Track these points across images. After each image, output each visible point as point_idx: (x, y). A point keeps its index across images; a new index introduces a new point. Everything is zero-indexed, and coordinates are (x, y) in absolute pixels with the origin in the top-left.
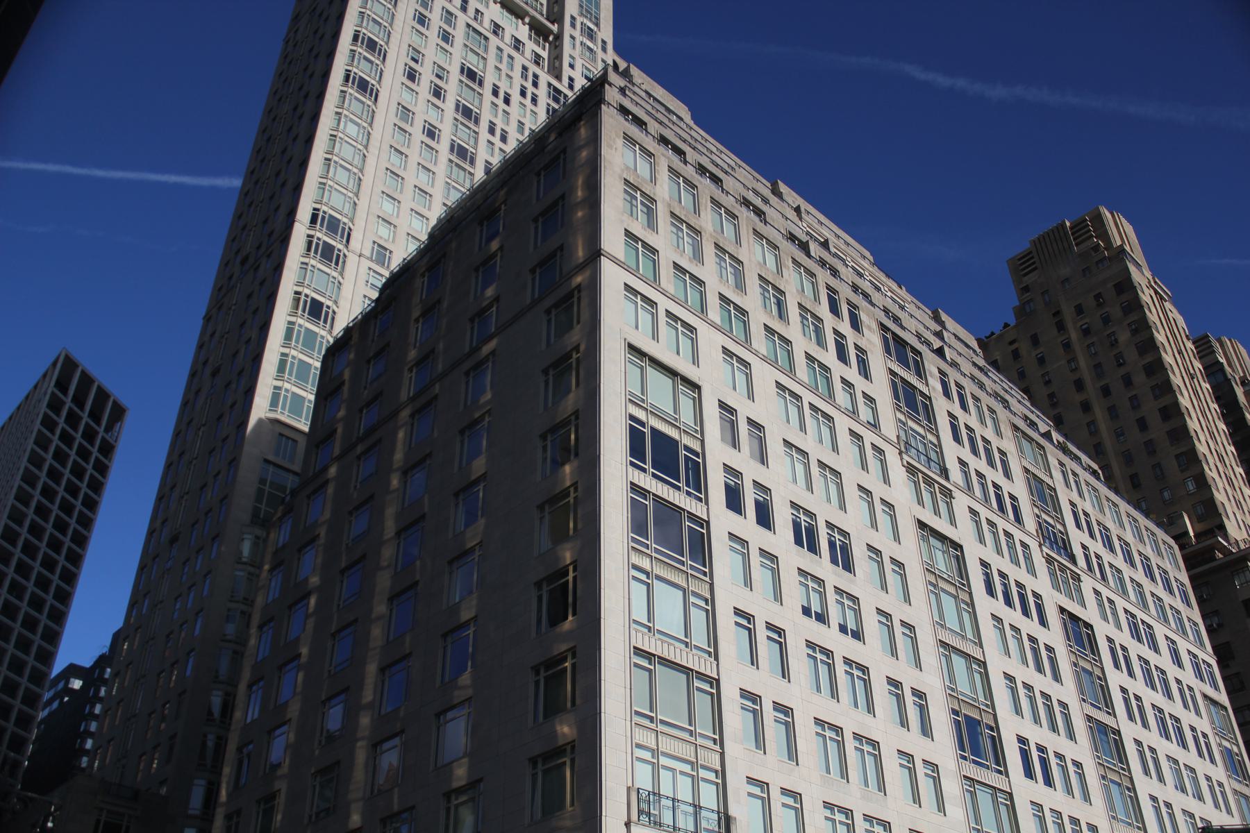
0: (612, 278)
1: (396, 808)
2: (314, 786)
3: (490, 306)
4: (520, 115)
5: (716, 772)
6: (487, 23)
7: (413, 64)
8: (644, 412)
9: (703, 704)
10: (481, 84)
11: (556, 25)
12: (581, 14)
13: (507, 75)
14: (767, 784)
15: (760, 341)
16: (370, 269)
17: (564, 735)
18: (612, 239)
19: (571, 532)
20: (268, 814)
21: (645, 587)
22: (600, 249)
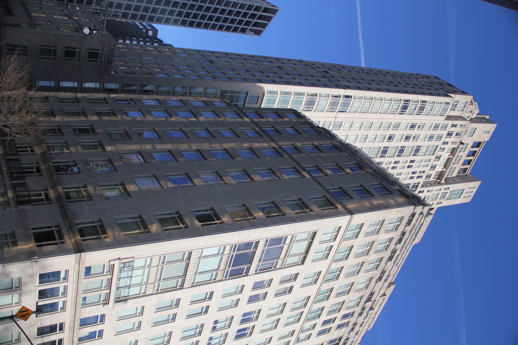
0: (343, 221)
1: (115, 164)
2: (120, 131)
3: (323, 173)
4: (402, 178)
5: (145, 293)
6: (440, 153)
7: (417, 126)
8: (289, 242)
9: (172, 283)
10: (414, 155)
11: (444, 182)
13: (420, 165)
14: (142, 315)
15: (326, 286)
16: (331, 122)
17: (152, 228)
18: (358, 218)
19: (235, 219)
20: (108, 114)
21: (217, 253)
22: (354, 214)
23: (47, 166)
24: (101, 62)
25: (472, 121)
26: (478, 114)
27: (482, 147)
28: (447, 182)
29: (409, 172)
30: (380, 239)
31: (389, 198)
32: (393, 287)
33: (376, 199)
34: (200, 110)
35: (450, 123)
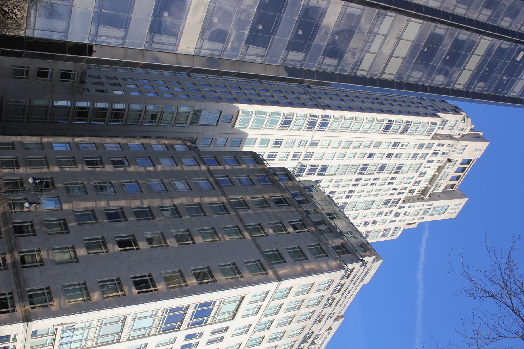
0: (271, 286)
2: (78, 184)
6: (424, 170)
7: (400, 145)
8: (218, 304)
10: (396, 172)
11: (428, 198)
12: (434, 208)
13: (401, 182)
15: (257, 335)
16: (308, 140)
18: (286, 284)
19: (170, 286)
22: (282, 281)
23: (7, 228)
24: (73, 82)
25: (463, 138)
26: (471, 130)
27: (472, 164)
28: (432, 197)
29: (390, 189)
30: (310, 297)
31: (323, 261)
32: (341, 321)
33: (310, 262)
34: (158, 156)
35: (437, 142)
